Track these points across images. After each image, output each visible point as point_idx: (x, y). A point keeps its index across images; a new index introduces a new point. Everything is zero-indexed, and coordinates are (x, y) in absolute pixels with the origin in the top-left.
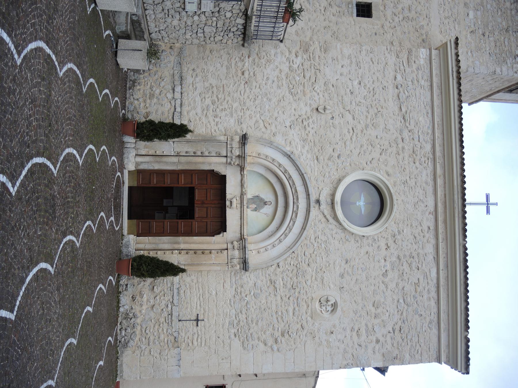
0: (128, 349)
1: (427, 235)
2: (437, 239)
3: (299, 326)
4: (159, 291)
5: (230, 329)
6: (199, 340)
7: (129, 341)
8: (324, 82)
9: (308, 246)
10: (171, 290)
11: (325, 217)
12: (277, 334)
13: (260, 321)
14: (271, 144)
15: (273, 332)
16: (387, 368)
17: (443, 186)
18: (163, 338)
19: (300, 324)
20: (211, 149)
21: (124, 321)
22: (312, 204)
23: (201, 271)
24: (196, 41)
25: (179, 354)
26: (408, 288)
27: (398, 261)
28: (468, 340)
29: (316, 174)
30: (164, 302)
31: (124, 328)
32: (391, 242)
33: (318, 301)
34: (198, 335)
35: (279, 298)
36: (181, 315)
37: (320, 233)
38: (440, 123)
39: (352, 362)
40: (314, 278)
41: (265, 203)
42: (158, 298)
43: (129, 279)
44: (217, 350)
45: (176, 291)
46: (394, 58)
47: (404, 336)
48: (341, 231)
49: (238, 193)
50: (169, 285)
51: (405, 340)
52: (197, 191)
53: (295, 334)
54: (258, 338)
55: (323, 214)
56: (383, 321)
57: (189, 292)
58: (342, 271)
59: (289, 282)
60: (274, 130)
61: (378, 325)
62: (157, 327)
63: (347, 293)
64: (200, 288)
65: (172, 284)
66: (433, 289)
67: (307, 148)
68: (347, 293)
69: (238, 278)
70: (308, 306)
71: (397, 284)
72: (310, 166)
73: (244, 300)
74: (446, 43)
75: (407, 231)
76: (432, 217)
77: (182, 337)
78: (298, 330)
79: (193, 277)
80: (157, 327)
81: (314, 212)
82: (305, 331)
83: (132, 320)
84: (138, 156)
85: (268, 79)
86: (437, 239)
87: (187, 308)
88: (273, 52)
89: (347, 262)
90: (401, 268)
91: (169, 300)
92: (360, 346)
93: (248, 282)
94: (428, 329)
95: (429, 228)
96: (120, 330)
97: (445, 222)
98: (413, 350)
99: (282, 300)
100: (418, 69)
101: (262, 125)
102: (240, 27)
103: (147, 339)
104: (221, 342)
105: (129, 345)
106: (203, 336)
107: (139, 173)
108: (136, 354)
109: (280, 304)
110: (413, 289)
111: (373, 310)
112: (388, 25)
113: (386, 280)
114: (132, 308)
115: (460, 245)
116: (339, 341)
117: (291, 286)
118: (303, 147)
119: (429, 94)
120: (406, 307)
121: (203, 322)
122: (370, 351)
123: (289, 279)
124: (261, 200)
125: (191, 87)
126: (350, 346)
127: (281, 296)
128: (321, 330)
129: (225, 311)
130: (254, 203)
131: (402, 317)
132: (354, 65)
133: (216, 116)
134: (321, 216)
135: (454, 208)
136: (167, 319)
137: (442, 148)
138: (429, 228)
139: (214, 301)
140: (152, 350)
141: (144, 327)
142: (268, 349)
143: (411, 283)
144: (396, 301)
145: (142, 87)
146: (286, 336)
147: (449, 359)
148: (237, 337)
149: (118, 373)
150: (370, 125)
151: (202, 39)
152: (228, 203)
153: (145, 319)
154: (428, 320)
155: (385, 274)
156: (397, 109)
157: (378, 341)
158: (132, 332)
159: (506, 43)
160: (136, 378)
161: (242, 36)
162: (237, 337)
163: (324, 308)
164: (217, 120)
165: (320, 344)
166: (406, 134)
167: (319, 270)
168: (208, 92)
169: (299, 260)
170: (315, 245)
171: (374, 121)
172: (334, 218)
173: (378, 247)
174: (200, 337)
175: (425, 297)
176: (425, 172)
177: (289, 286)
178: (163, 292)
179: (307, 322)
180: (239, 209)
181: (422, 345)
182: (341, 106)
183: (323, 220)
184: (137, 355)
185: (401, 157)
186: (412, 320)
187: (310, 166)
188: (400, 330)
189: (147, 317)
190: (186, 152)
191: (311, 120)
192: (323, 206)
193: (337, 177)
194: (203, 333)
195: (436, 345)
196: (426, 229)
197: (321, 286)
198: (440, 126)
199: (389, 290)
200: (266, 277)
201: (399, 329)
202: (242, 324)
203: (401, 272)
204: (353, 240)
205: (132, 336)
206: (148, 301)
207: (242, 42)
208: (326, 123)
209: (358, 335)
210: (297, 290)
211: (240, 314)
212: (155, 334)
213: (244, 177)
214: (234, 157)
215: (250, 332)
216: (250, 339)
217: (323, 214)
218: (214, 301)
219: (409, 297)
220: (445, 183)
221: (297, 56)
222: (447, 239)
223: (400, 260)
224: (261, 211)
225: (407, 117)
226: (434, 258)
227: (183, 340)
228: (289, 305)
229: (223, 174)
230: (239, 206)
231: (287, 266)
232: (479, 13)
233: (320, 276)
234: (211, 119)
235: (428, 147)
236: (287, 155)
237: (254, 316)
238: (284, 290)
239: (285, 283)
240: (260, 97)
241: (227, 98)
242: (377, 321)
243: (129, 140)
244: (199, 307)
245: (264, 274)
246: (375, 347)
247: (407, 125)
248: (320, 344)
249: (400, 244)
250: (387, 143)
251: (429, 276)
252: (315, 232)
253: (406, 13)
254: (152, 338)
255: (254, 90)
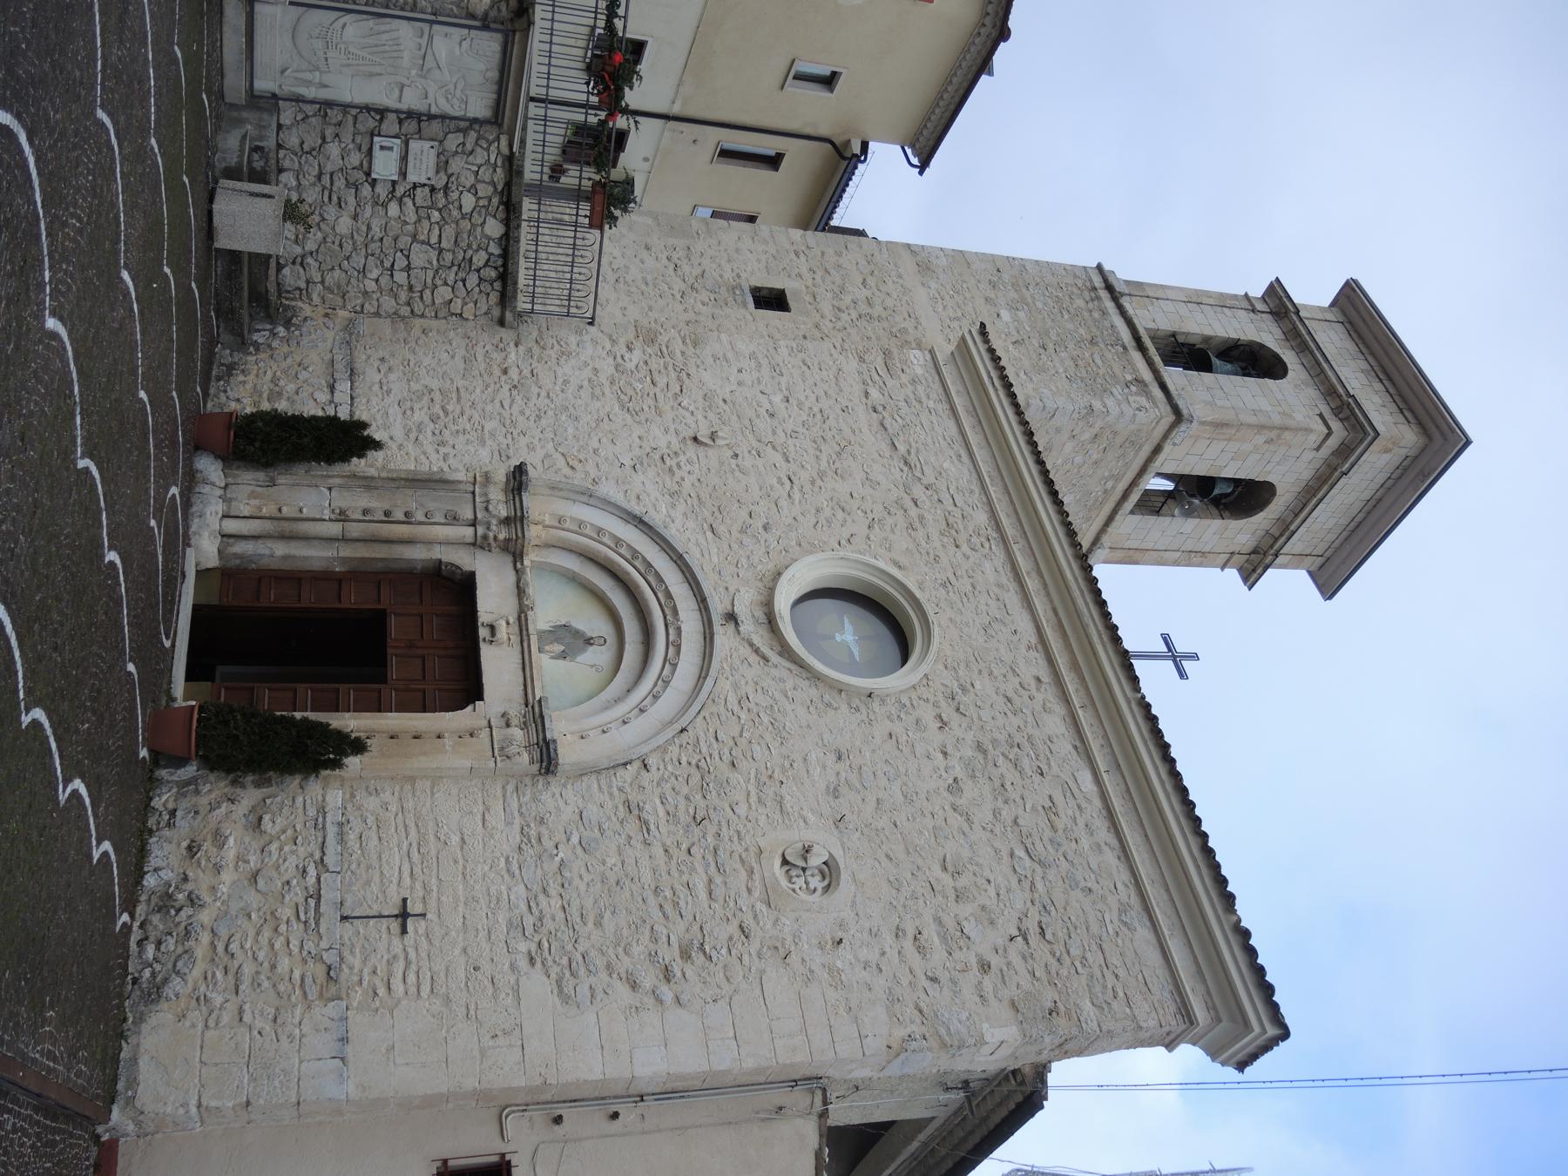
0: (164, 1005)
1: (1039, 697)
2: (1066, 700)
3: (733, 928)
4: (277, 828)
5: (512, 943)
6: (412, 978)
7: (166, 981)
8: (701, 393)
9: (723, 718)
10: (319, 826)
11: (757, 651)
12: (670, 954)
13: (607, 915)
14: (588, 496)
15: (652, 947)
16: (1041, 1072)
17: (1042, 592)
18: (287, 969)
19: (736, 923)
20: (432, 505)
21: (156, 919)
22: (717, 620)
23: (412, 779)
24: (388, 304)
25: (341, 1019)
26: (1026, 821)
27: (981, 757)
28: (1246, 934)
29: (715, 559)
30: (292, 861)
31: (152, 939)
32: (948, 712)
33: (778, 861)
34: (408, 963)
35: (658, 851)
36: (348, 904)
37: (750, 690)
38: (995, 474)
39: (924, 1029)
40: (753, 799)
41: (589, 642)
42: (274, 847)
43: (184, 795)
44: (472, 1007)
45: (332, 831)
46: (854, 363)
47: (1059, 949)
48: (807, 683)
49: (509, 608)
50: (312, 812)
51: (1067, 961)
52: (393, 621)
53: (724, 951)
54: (609, 966)
55: (751, 645)
56: (983, 908)
57: (375, 838)
58: (833, 779)
59: (682, 807)
60: (593, 473)
61: (972, 919)
62: (267, 934)
63: (858, 834)
64: (412, 825)
65: (322, 810)
66: (1100, 825)
67: (681, 507)
68: (858, 834)
69: (527, 798)
70: (751, 872)
71: (996, 813)
72: (697, 544)
73: (552, 857)
74: (963, 338)
75: (982, 685)
76: (1038, 657)
77: (351, 968)
78: (731, 938)
79: (386, 796)
80: (267, 934)
81: (724, 638)
82: (755, 946)
83: (183, 914)
84: (228, 518)
85: (566, 382)
86: (1066, 700)
87: (368, 883)
88: (573, 339)
89: (840, 758)
90: (996, 773)
91: (312, 855)
92: (934, 980)
93: (558, 808)
94: (1125, 929)
95: (1038, 680)
96: (140, 943)
97: (1075, 666)
98: (1098, 988)
99: (671, 857)
100: (913, 382)
101: (561, 462)
102: (495, 249)
103: (231, 977)
104: (487, 983)
105: (168, 991)
106: (425, 964)
107: (228, 575)
108: (188, 1023)
109: (664, 868)
110: (1042, 821)
111: (946, 879)
112: (830, 325)
113: (962, 802)
114: (185, 879)
115: (1129, 702)
116: (866, 966)
117: (690, 819)
118: (673, 506)
119: (951, 424)
120: (1039, 869)
121: (423, 923)
122: (968, 994)
123: (682, 802)
124: (577, 634)
125: (376, 388)
126: (905, 982)
127: (664, 845)
128: (804, 937)
129: (493, 890)
130: (558, 640)
131: (1036, 895)
132: (766, 371)
133: (442, 443)
134: (746, 651)
135: (1085, 628)
136: (302, 910)
137: (1014, 520)
138: (1038, 680)
139: (456, 862)
140: (247, 1007)
141: (223, 933)
142: (645, 999)
143: (1034, 809)
144: (1006, 858)
145: (251, 377)
146: (699, 959)
147: (1217, 1011)
148: (539, 964)
149: (120, 1086)
150: (831, 473)
151: (403, 296)
152: (483, 633)
153: (226, 913)
154: (1112, 900)
155: (955, 787)
156: (887, 451)
157: (985, 967)
158: (180, 950)
159: (1099, 362)
160: (185, 1105)
161: (498, 285)
162: (539, 964)
163: (800, 882)
164: (442, 450)
165: (809, 977)
166: (918, 491)
167: (764, 779)
168: (420, 398)
169: (704, 750)
170: (743, 716)
171: (838, 465)
172: (780, 654)
173: (917, 722)
174: (414, 967)
175: (1085, 843)
176: (988, 566)
177: (684, 818)
178: (290, 832)
179: (755, 916)
180: (517, 648)
181: (1121, 973)
182: (751, 437)
183: (753, 658)
184: (193, 1026)
185: (921, 533)
186: (1067, 903)
187: (697, 544)
188: (1043, 932)
189: (235, 906)
190: (365, 512)
191: (682, 458)
192: (747, 627)
193: (771, 566)
194: (424, 955)
195: (1162, 972)
196: (1033, 684)
197: (777, 816)
198: (997, 480)
199: (976, 826)
200: (611, 794)
201: (1038, 930)
202: (549, 925)
203: (997, 783)
204: (844, 708)
205: (180, 964)
206: (241, 858)
207: (496, 312)
208: (722, 464)
209: (920, 950)
210: (712, 829)
211: (541, 897)
212: (261, 956)
213: (524, 572)
214: (494, 522)
215: (581, 949)
216: (582, 971)
217: (751, 645)
218: (456, 862)
219: (1037, 842)
220: (1045, 585)
221: (629, 349)
222: (1093, 704)
223: (985, 752)
224: (579, 659)
225: (913, 459)
226: (1075, 747)
227: (356, 979)
228: (693, 870)
229: (467, 568)
230: (515, 639)
231: (670, 768)
232: (1021, 314)
233: (771, 794)
234: (430, 449)
235: (982, 517)
236: (635, 517)
237: (589, 903)
238: (672, 828)
239: (671, 810)
240: (550, 413)
241: (468, 412)
242: (966, 910)
243: (209, 467)
244: (407, 880)
245: (605, 788)
246: (980, 983)
247: (918, 474)
248: (809, 977)
249: (975, 717)
250: (878, 508)
251: (1076, 791)
252: (736, 686)
253: (863, 308)
254: (248, 969)
255: (534, 400)
